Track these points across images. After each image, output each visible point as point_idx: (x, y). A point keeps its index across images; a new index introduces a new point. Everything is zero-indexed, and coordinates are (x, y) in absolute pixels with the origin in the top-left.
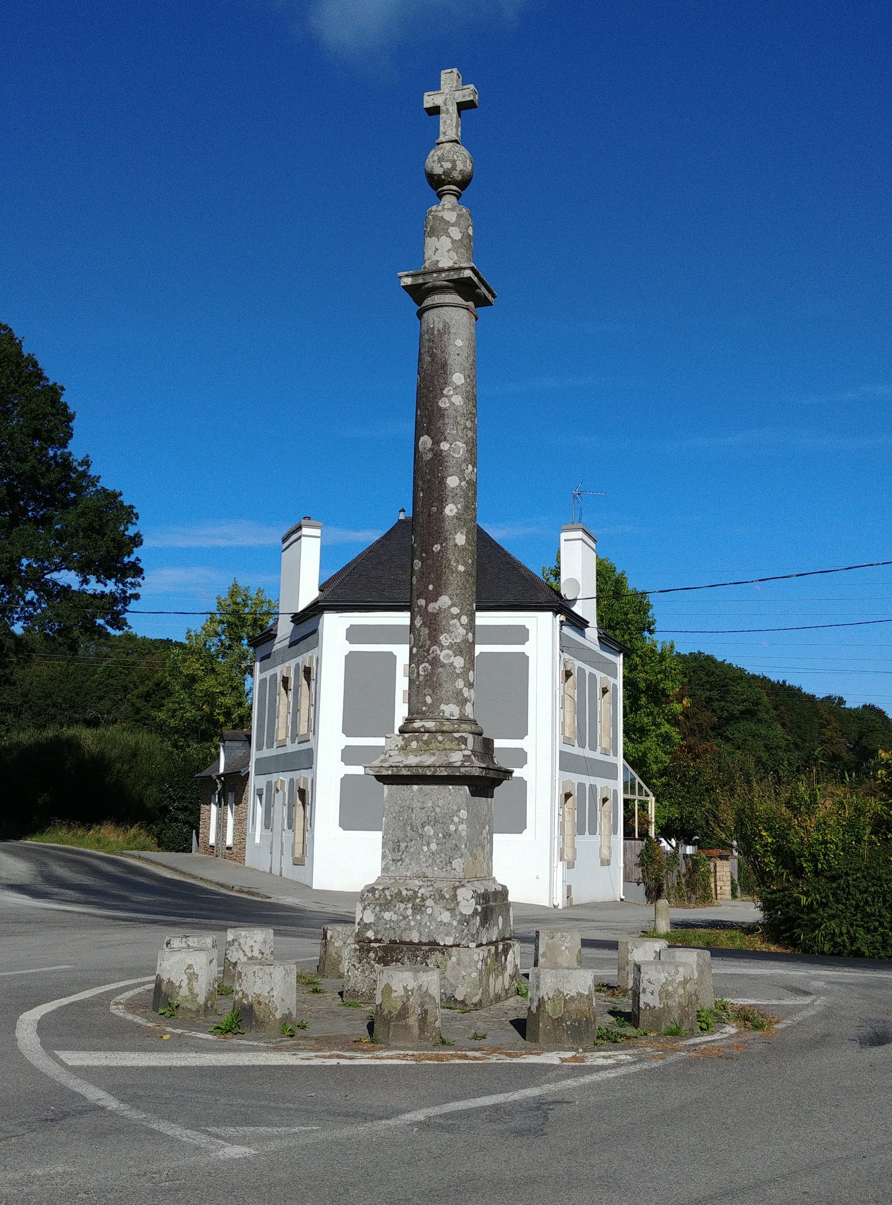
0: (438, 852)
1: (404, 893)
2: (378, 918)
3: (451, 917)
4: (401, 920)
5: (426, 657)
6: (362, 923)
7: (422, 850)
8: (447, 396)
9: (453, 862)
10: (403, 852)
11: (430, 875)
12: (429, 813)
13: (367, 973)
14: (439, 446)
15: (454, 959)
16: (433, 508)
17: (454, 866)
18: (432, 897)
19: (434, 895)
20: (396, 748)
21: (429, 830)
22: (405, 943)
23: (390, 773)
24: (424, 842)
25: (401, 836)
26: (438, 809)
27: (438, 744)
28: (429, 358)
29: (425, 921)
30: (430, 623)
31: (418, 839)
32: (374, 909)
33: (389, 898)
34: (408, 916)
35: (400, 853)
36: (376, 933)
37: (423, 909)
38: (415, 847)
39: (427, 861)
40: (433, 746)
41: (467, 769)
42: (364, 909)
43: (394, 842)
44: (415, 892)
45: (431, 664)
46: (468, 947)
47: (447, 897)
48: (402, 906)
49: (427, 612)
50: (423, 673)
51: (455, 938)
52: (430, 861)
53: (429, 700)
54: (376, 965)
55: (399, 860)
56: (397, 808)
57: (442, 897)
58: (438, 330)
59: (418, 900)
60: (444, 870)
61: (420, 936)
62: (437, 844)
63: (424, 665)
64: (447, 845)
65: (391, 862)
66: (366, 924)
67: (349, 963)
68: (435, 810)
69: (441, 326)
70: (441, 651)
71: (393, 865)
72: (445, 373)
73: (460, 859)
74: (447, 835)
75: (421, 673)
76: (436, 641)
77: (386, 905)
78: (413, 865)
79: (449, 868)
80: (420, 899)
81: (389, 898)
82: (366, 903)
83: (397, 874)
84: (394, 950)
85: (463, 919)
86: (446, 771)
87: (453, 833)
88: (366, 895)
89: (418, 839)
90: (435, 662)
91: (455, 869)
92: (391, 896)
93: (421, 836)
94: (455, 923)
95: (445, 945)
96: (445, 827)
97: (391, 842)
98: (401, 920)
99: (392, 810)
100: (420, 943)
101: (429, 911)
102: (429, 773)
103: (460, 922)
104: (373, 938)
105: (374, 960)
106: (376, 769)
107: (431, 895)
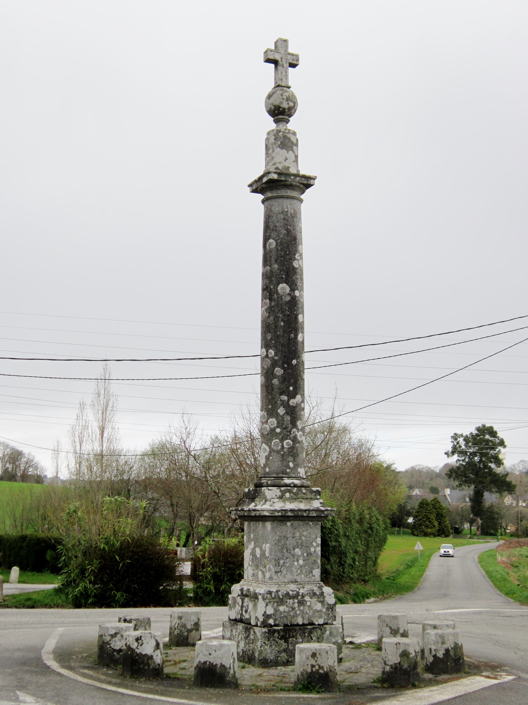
0: (304, 566)
1: (291, 593)
2: (276, 610)
3: (322, 606)
4: (291, 611)
5: (289, 436)
6: (265, 615)
7: (294, 564)
8: (297, 260)
9: (313, 572)
10: (282, 566)
11: (299, 581)
12: (298, 540)
13: (273, 647)
14: (294, 293)
15: (328, 632)
16: (292, 335)
17: (314, 574)
18: (309, 595)
19: (310, 593)
20: (276, 497)
21: (298, 551)
22: (294, 625)
23: (280, 514)
24: (295, 559)
25: (280, 555)
26: (303, 538)
27: (303, 495)
28: (285, 231)
29: (306, 610)
30: (291, 413)
31: (291, 557)
32: (273, 604)
33: (281, 597)
34: (295, 608)
35: (280, 567)
36: (275, 620)
37: (305, 603)
38: (289, 563)
39: (297, 571)
40: (300, 495)
41: (329, 512)
42: (267, 605)
43: (275, 560)
44: (298, 593)
45: (293, 441)
46: (332, 624)
47: (318, 594)
48: (291, 601)
49: (289, 405)
50: (287, 447)
51: (325, 619)
52: (299, 571)
53: (291, 465)
54: (280, 641)
55: (278, 572)
56: (277, 538)
57: (315, 594)
58: (291, 214)
59: (300, 597)
60: (308, 576)
61: (303, 620)
62: (304, 560)
63: (287, 441)
64: (310, 561)
65: (274, 573)
66: (268, 615)
67: (261, 641)
68: (301, 539)
69: (292, 212)
70: (298, 432)
71: (275, 575)
72: (296, 243)
73: (317, 569)
74: (309, 554)
75: (285, 446)
76: (295, 426)
77: (281, 601)
78: (289, 574)
79: (311, 575)
80: (301, 597)
81: (281, 597)
82: (267, 601)
83: (278, 581)
84: (290, 630)
85: (329, 607)
86: (316, 513)
87: (313, 553)
88: (266, 596)
89: (291, 557)
90: (295, 440)
91: (314, 576)
92: (283, 595)
93: (293, 556)
94: (324, 610)
95: (319, 625)
96: (308, 549)
97: (273, 560)
98: (291, 611)
99: (273, 538)
100: (304, 625)
101: (308, 604)
102: (305, 515)
103: (328, 609)
104: (273, 624)
105: (278, 638)
106: (271, 512)
107: (308, 594)
